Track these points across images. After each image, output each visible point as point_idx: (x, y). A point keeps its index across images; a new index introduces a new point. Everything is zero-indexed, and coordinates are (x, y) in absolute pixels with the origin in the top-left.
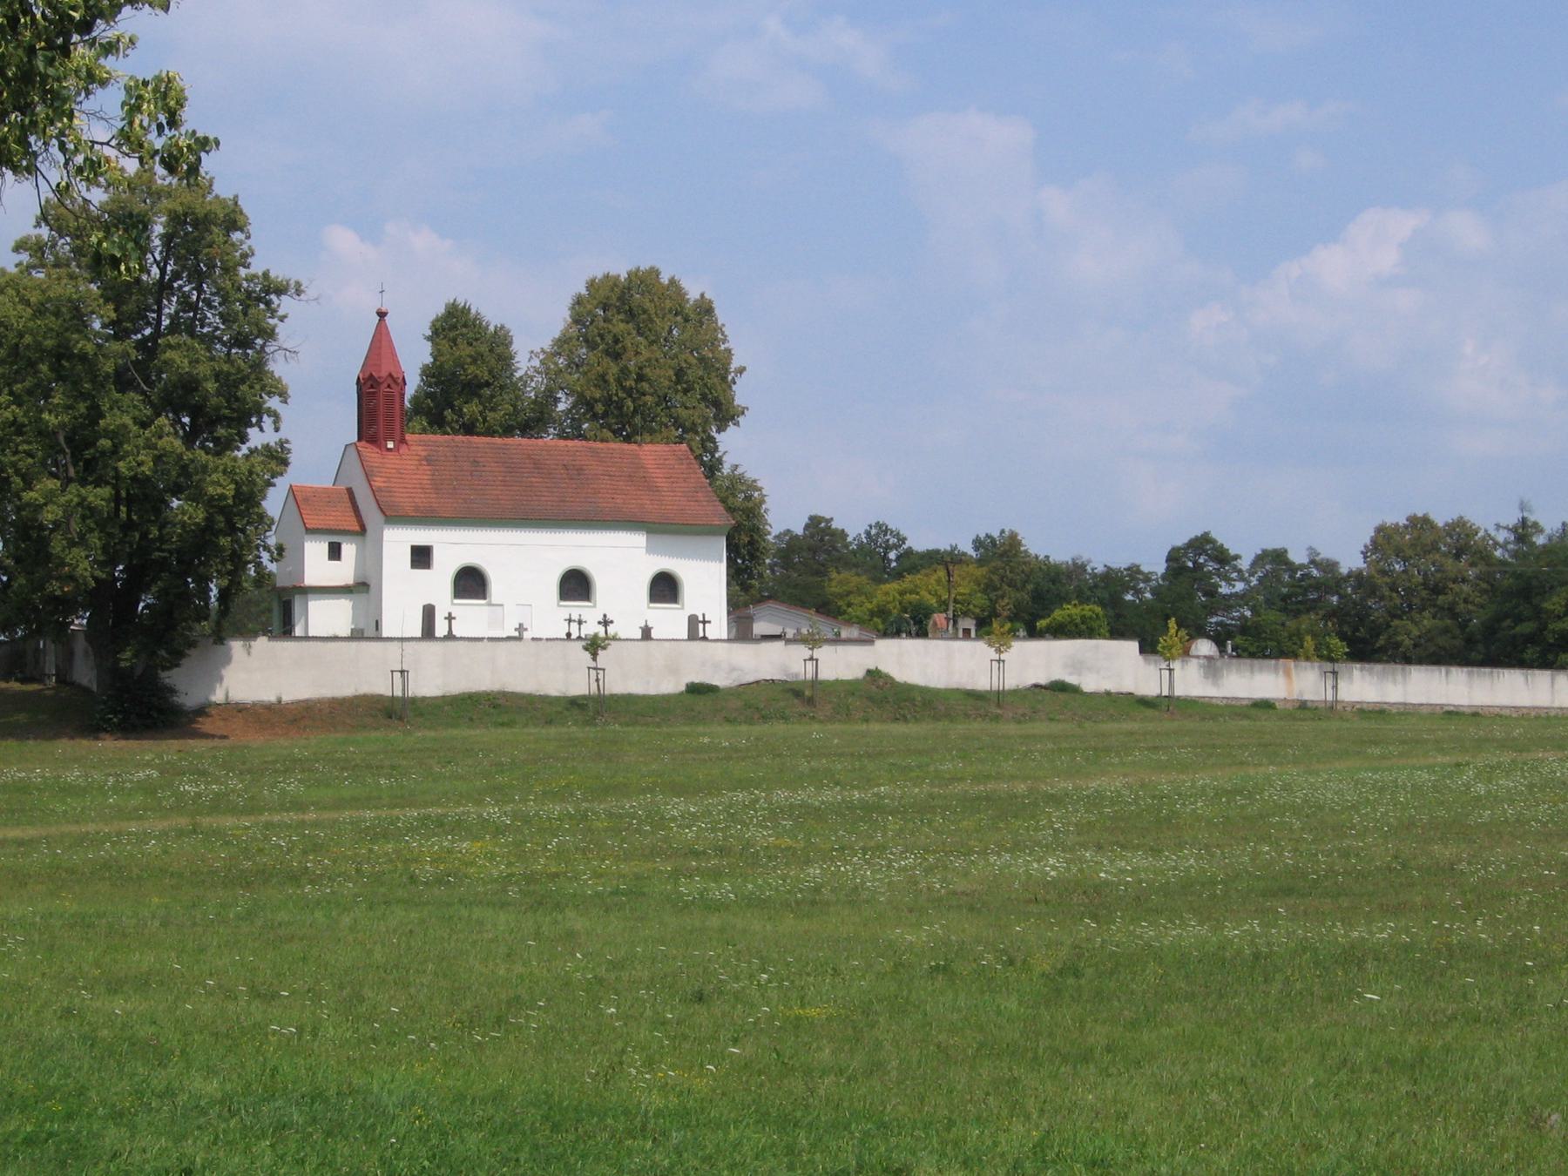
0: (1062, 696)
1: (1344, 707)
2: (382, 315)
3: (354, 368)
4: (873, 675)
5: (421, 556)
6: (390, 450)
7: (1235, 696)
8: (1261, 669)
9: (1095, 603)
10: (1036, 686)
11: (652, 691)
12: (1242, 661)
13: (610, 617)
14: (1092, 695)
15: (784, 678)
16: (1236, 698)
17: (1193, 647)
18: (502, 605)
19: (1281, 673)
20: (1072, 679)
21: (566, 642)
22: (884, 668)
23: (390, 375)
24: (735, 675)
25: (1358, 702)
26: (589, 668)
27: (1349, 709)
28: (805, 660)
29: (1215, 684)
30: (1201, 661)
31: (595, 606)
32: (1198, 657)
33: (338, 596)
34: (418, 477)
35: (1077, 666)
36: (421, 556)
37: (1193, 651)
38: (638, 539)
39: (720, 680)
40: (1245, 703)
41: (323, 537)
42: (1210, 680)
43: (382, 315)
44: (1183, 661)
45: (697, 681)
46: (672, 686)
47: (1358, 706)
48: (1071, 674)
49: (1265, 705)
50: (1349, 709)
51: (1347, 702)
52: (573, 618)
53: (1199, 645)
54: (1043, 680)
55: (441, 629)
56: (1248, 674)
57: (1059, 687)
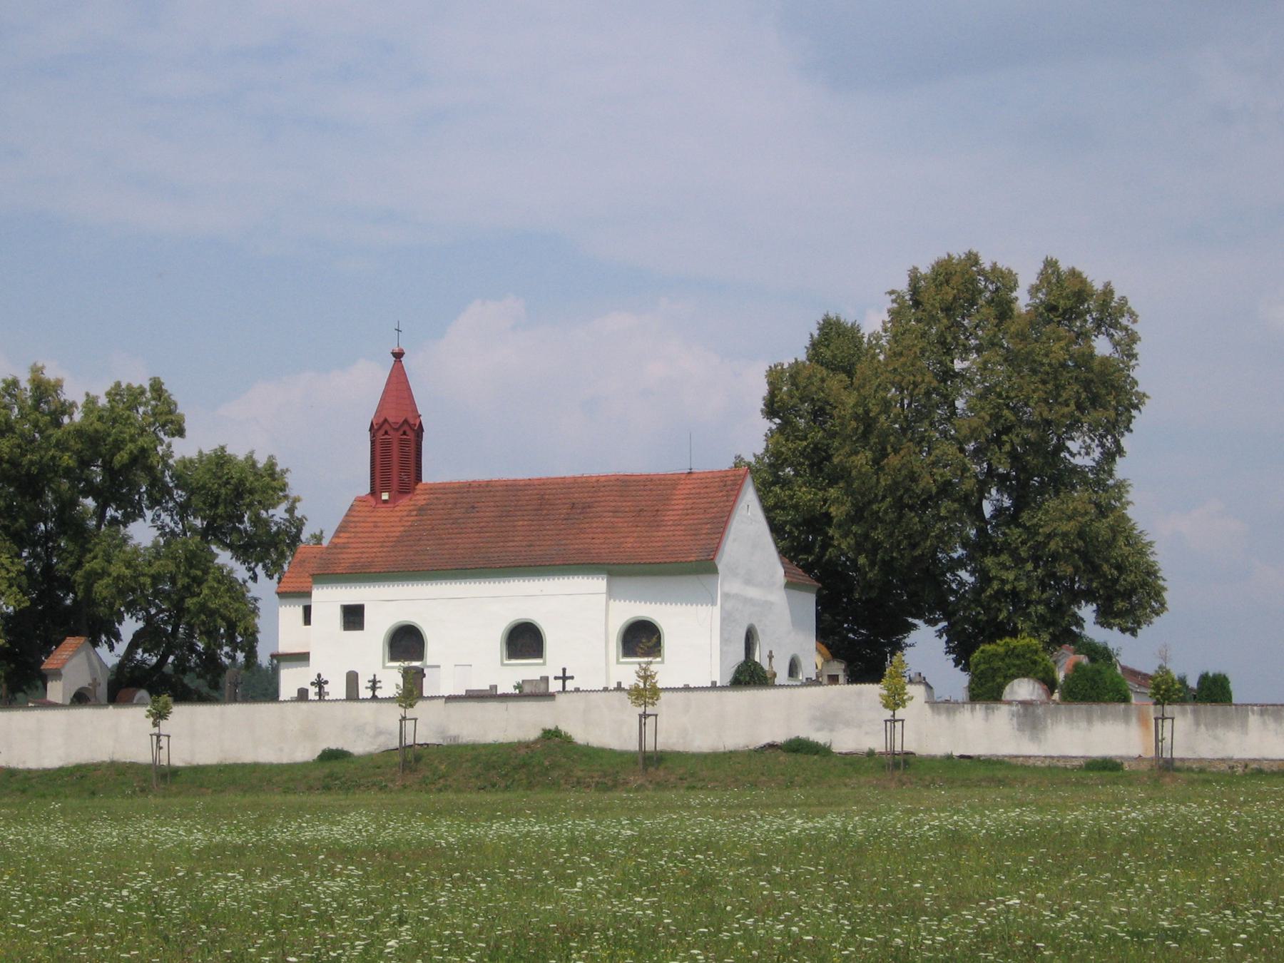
0: (800, 758)
1: (1232, 768)
2: (398, 355)
3: (368, 413)
4: (552, 736)
5: (353, 617)
6: (385, 501)
7: (1062, 754)
8: (1103, 718)
9: (983, 642)
10: (772, 746)
11: (285, 759)
12: (1075, 706)
13: (324, 677)
14: (360, 757)
15: (441, 741)
16: (1064, 757)
17: (1007, 689)
18: (438, 667)
19: (1134, 720)
20: (819, 737)
21: (318, 703)
22: (564, 728)
23: (406, 421)
24: (382, 739)
25: (1254, 760)
26: (151, 735)
27: (1240, 770)
28: (886, 721)
29: (1035, 738)
30: (1014, 708)
31: (544, 664)
32: (1010, 703)
33: (294, 663)
34: (389, 524)
35: (828, 719)
36: (353, 617)
37: (1008, 693)
38: (596, 584)
39: (358, 747)
40: (1076, 763)
41: (294, 600)
42: (1027, 733)
43: (398, 355)
44: (987, 708)
45: (334, 747)
46: (305, 753)
47: (1254, 766)
48: (819, 730)
49: (1107, 766)
50: (1240, 770)
51: (1238, 761)
52: (568, 682)
53: (1016, 687)
54: (780, 737)
55: (365, 693)
56: (1083, 725)
57: (798, 747)
